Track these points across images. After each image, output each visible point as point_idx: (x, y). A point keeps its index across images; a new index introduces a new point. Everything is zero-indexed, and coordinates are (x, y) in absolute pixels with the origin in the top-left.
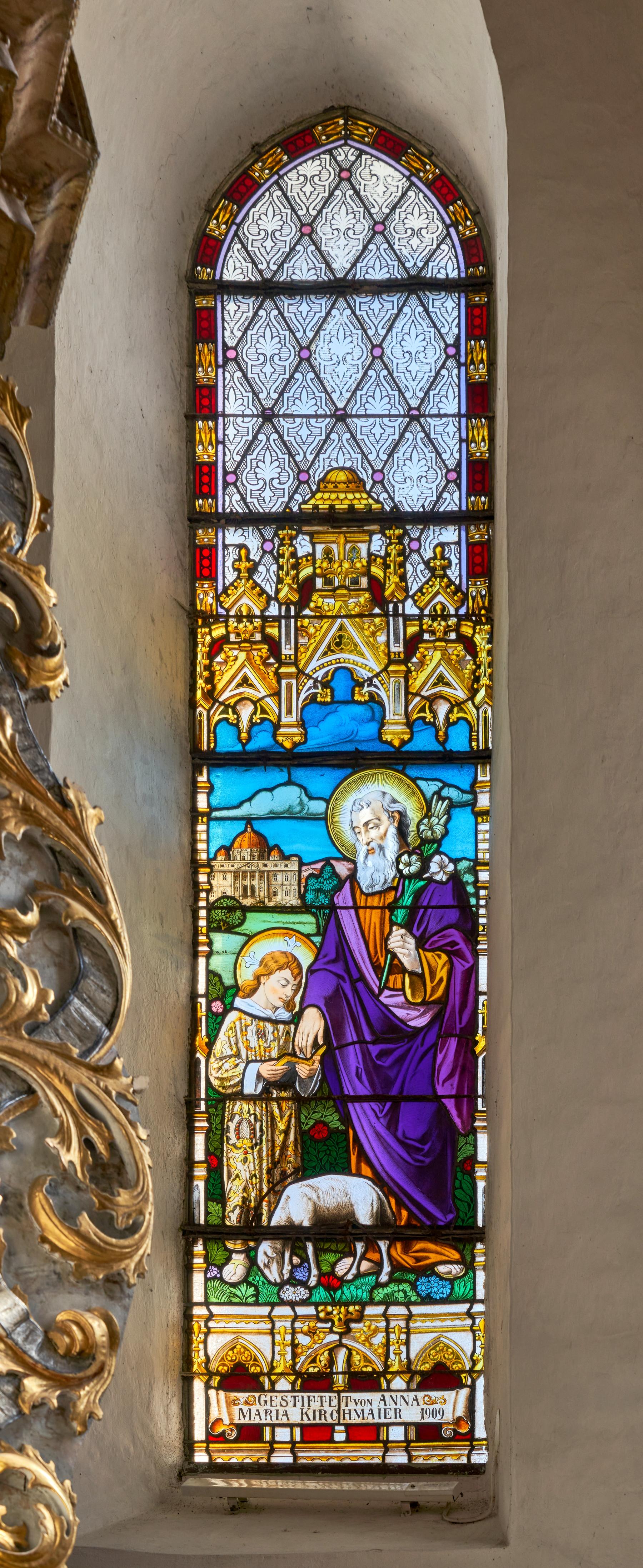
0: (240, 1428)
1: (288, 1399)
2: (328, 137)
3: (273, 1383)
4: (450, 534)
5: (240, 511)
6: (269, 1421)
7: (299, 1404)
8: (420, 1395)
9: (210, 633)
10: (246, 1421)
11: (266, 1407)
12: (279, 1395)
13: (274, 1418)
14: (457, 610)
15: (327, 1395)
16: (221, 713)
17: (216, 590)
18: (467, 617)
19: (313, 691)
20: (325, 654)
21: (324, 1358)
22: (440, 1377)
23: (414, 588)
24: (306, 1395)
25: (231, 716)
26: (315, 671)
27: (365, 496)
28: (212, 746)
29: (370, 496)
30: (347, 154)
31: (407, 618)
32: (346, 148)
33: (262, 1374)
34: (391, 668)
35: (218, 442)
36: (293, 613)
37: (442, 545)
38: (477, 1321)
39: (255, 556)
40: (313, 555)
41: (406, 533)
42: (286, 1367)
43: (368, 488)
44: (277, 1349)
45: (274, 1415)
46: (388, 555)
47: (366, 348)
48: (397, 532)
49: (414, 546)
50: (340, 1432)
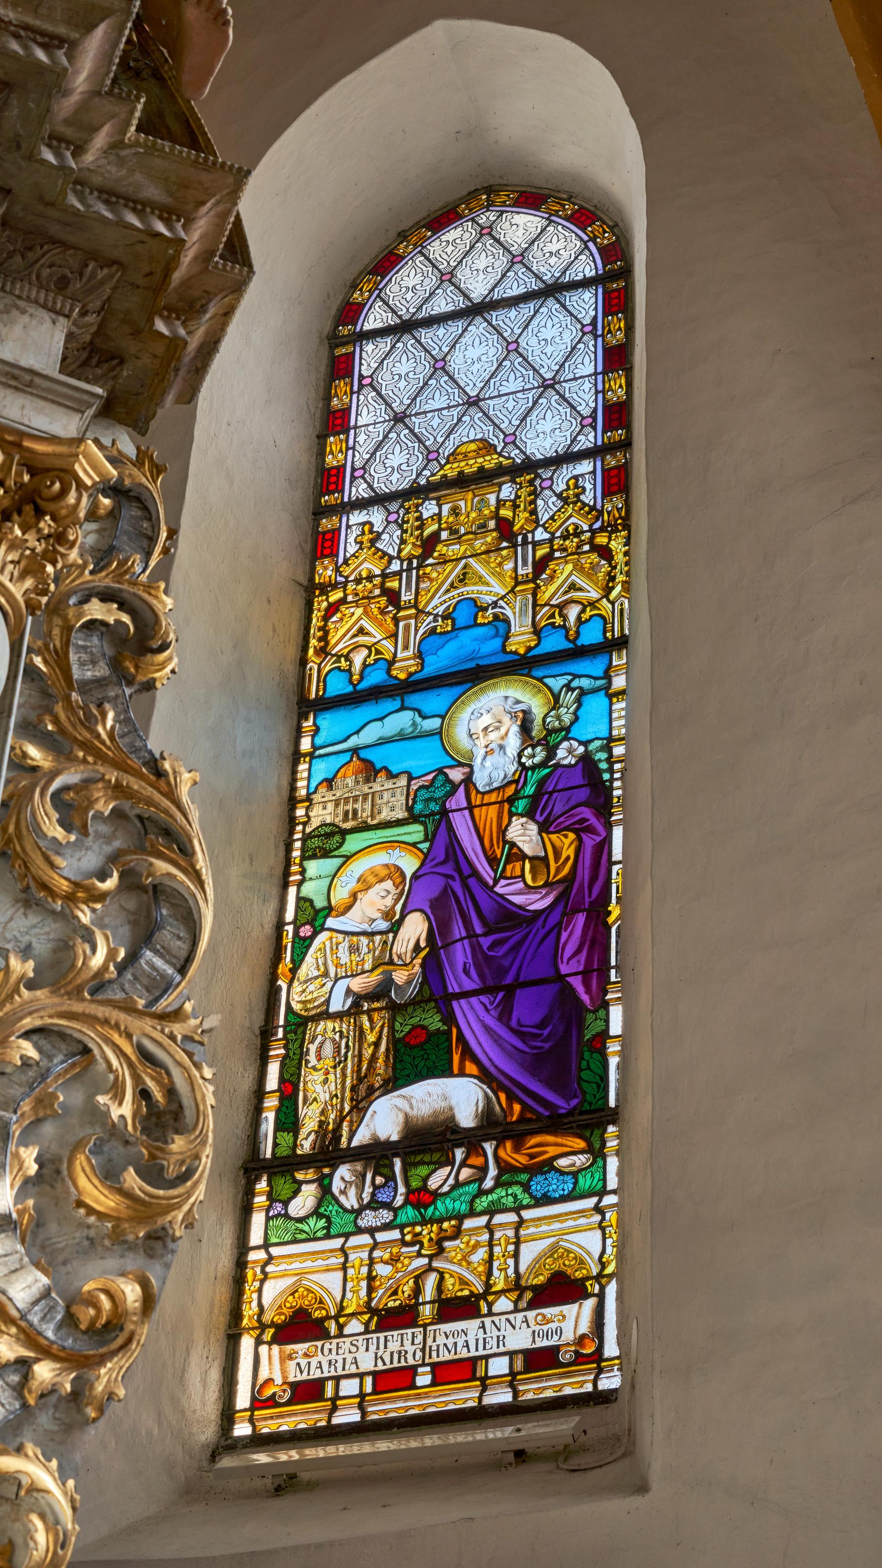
1: (359, 1344)
3: (341, 1327)
4: (585, 467)
6: (333, 1373)
7: (372, 1348)
8: (531, 1314)
11: (330, 1357)
13: (340, 1369)
14: (591, 526)
15: (409, 1331)
24: (382, 1335)
33: (328, 1317)
37: (576, 478)
38: (608, 1216)
41: (538, 476)
43: (499, 450)
50: (424, 1374)
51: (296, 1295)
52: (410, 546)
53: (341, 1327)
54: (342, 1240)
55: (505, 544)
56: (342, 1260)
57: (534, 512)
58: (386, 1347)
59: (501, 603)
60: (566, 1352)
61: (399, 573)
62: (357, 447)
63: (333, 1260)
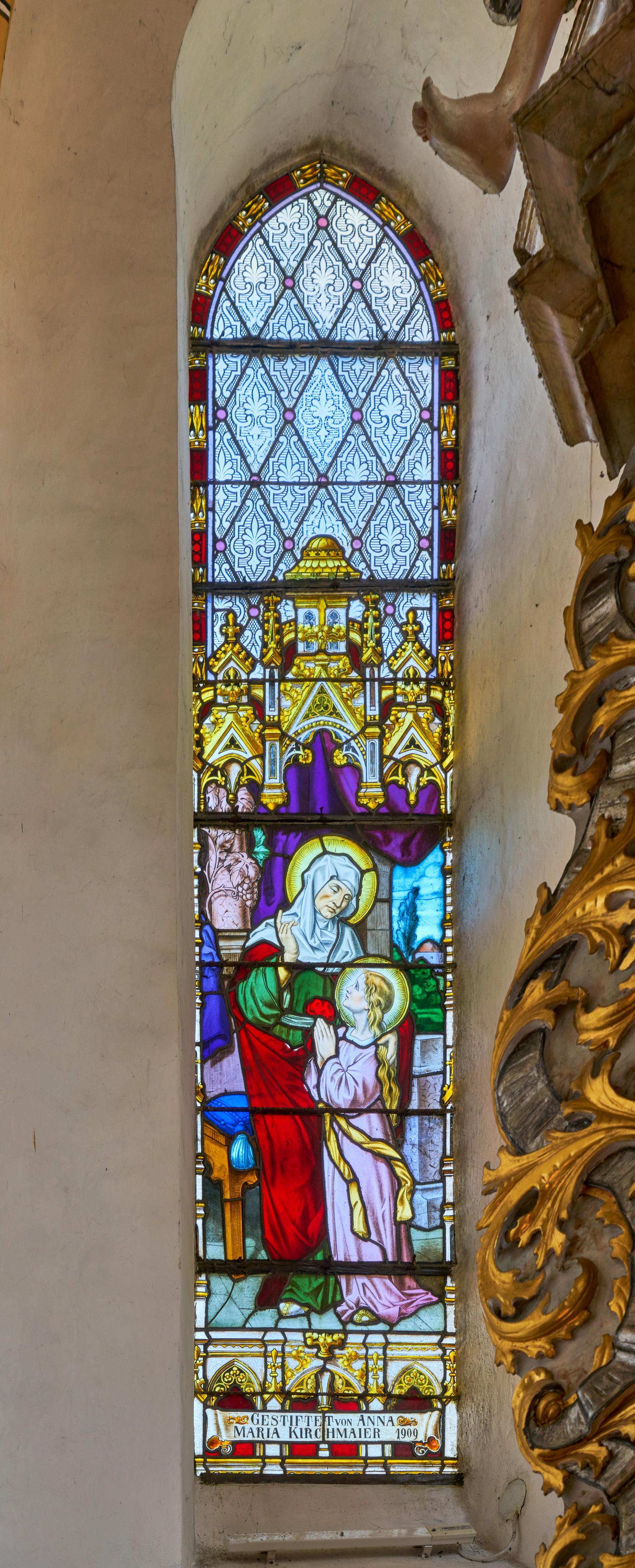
0: (235, 1444)
1: (278, 1420)
2: (306, 180)
3: (265, 1403)
4: (423, 601)
6: (260, 1439)
7: (288, 1424)
8: (395, 1416)
9: (199, 697)
11: (258, 1426)
12: (270, 1414)
13: (265, 1435)
14: (428, 673)
15: (313, 1415)
16: (210, 776)
17: (206, 654)
18: (437, 681)
19: (295, 752)
20: (306, 717)
21: (311, 1383)
22: (415, 1401)
24: (294, 1415)
25: (219, 778)
26: (297, 734)
27: (344, 564)
28: (202, 807)
29: (349, 565)
30: (321, 198)
31: (382, 681)
32: (322, 192)
33: (255, 1394)
34: (368, 730)
35: (208, 509)
36: (276, 677)
37: (414, 610)
38: (448, 1352)
39: (242, 619)
40: (295, 620)
41: (382, 598)
42: (276, 1387)
43: (347, 555)
46: (366, 620)
48: (373, 596)
49: (390, 610)
50: (323, 1449)
51: (232, 1373)
53: (265, 1403)
54: (262, 1333)
56: (263, 1350)
59: (353, 743)
60: (420, 1448)
61: (262, 682)
62: (217, 508)
63: (256, 1349)
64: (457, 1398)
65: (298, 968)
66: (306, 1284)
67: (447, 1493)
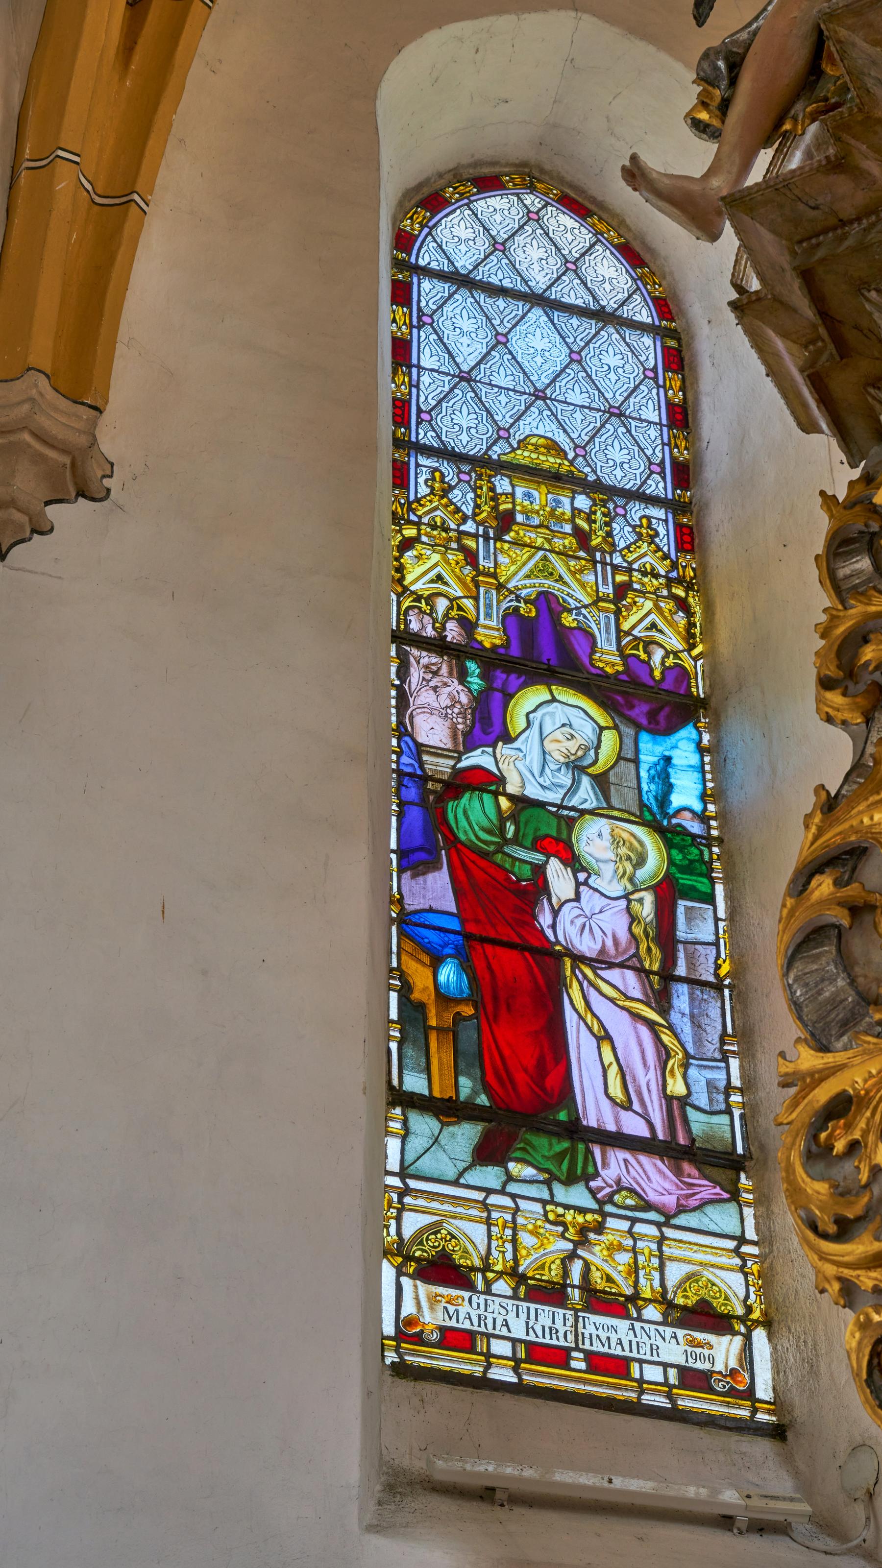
1: (509, 1308)
3: (488, 1284)
5: (436, 445)
6: (482, 1329)
7: (523, 1316)
8: (681, 1333)
9: (400, 531)
10: (453, 1323)
11: (478, 1312)
12: (497, 1300)
13: (490, 1326)
15: (561, 1311)
20: (528, 577)
22: (705, 1317)
23: (622, 544)
24: (533, 1306)
28: (402, 627)
31: (616, 568)
40: (513, 495)
44: (494, 1244)
45: (490, 1322)
47: (565, 350)
51: (439, 1236)
52: (600, 539)
53: (488, 1284)
55: (582, 554)
57: (610, 534)
58: (536, 1320)
64: (767, 1323)
65: (521, 802)
66: (546, 1146)
67: (762, 1447)
